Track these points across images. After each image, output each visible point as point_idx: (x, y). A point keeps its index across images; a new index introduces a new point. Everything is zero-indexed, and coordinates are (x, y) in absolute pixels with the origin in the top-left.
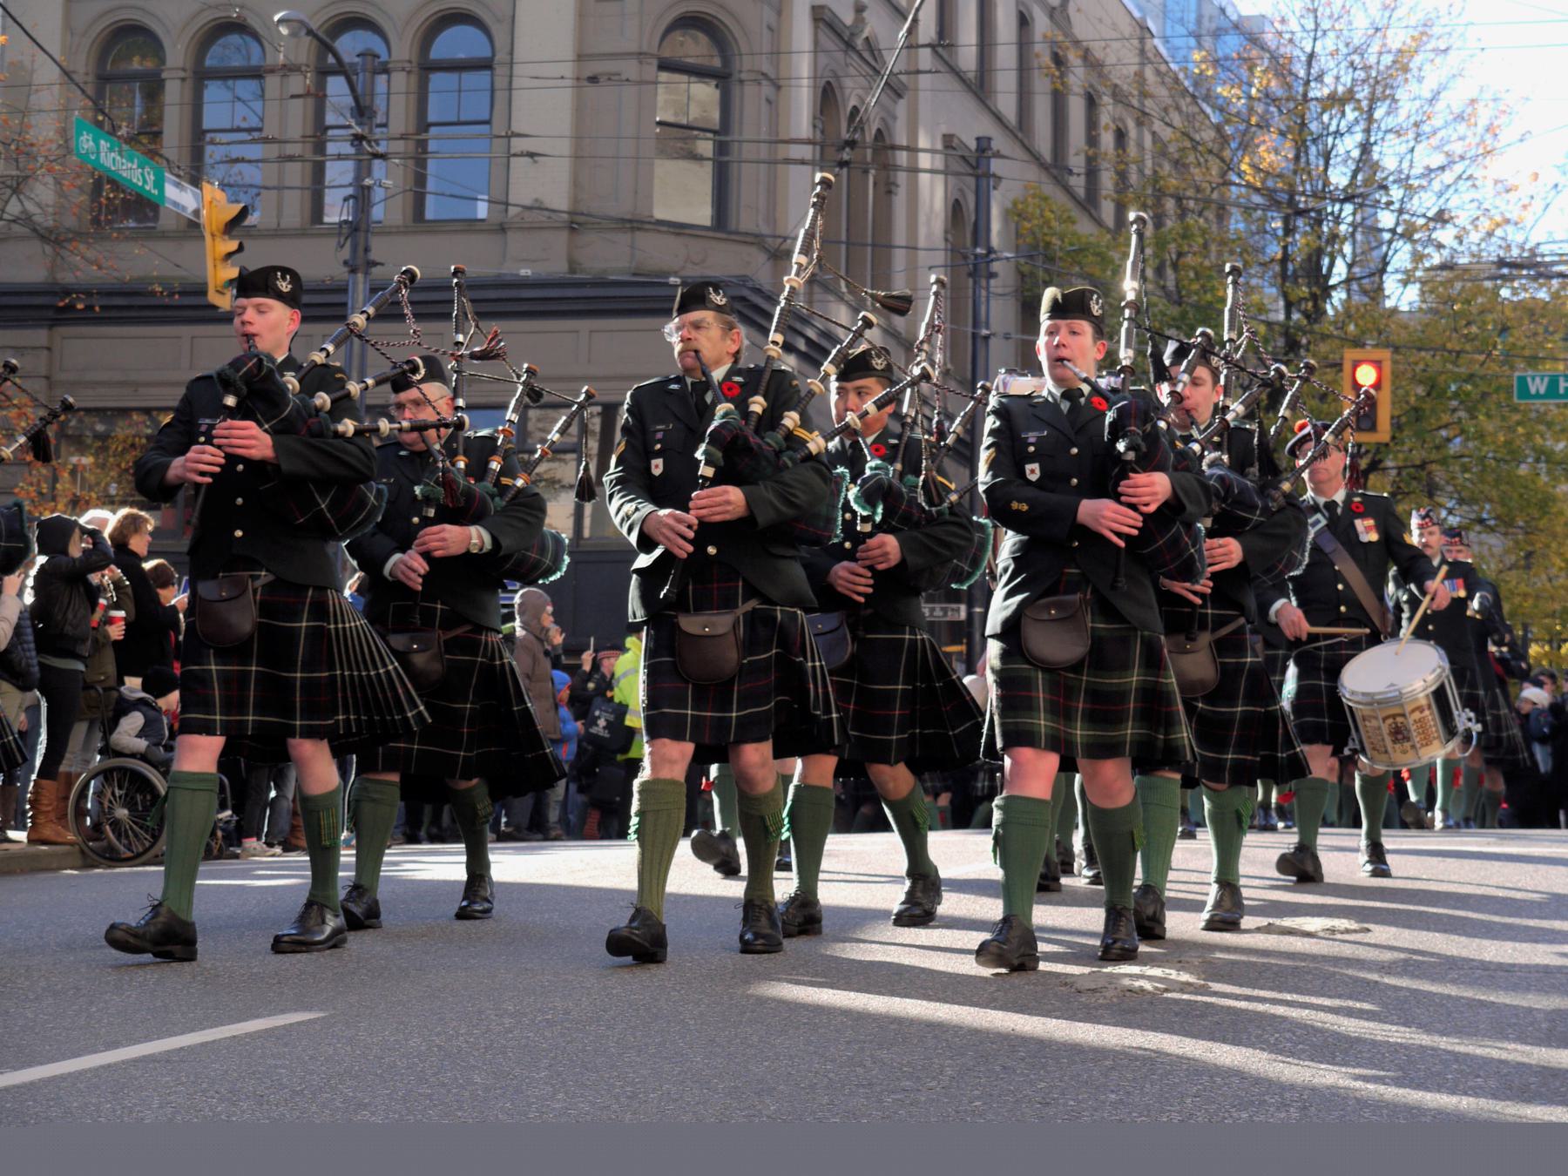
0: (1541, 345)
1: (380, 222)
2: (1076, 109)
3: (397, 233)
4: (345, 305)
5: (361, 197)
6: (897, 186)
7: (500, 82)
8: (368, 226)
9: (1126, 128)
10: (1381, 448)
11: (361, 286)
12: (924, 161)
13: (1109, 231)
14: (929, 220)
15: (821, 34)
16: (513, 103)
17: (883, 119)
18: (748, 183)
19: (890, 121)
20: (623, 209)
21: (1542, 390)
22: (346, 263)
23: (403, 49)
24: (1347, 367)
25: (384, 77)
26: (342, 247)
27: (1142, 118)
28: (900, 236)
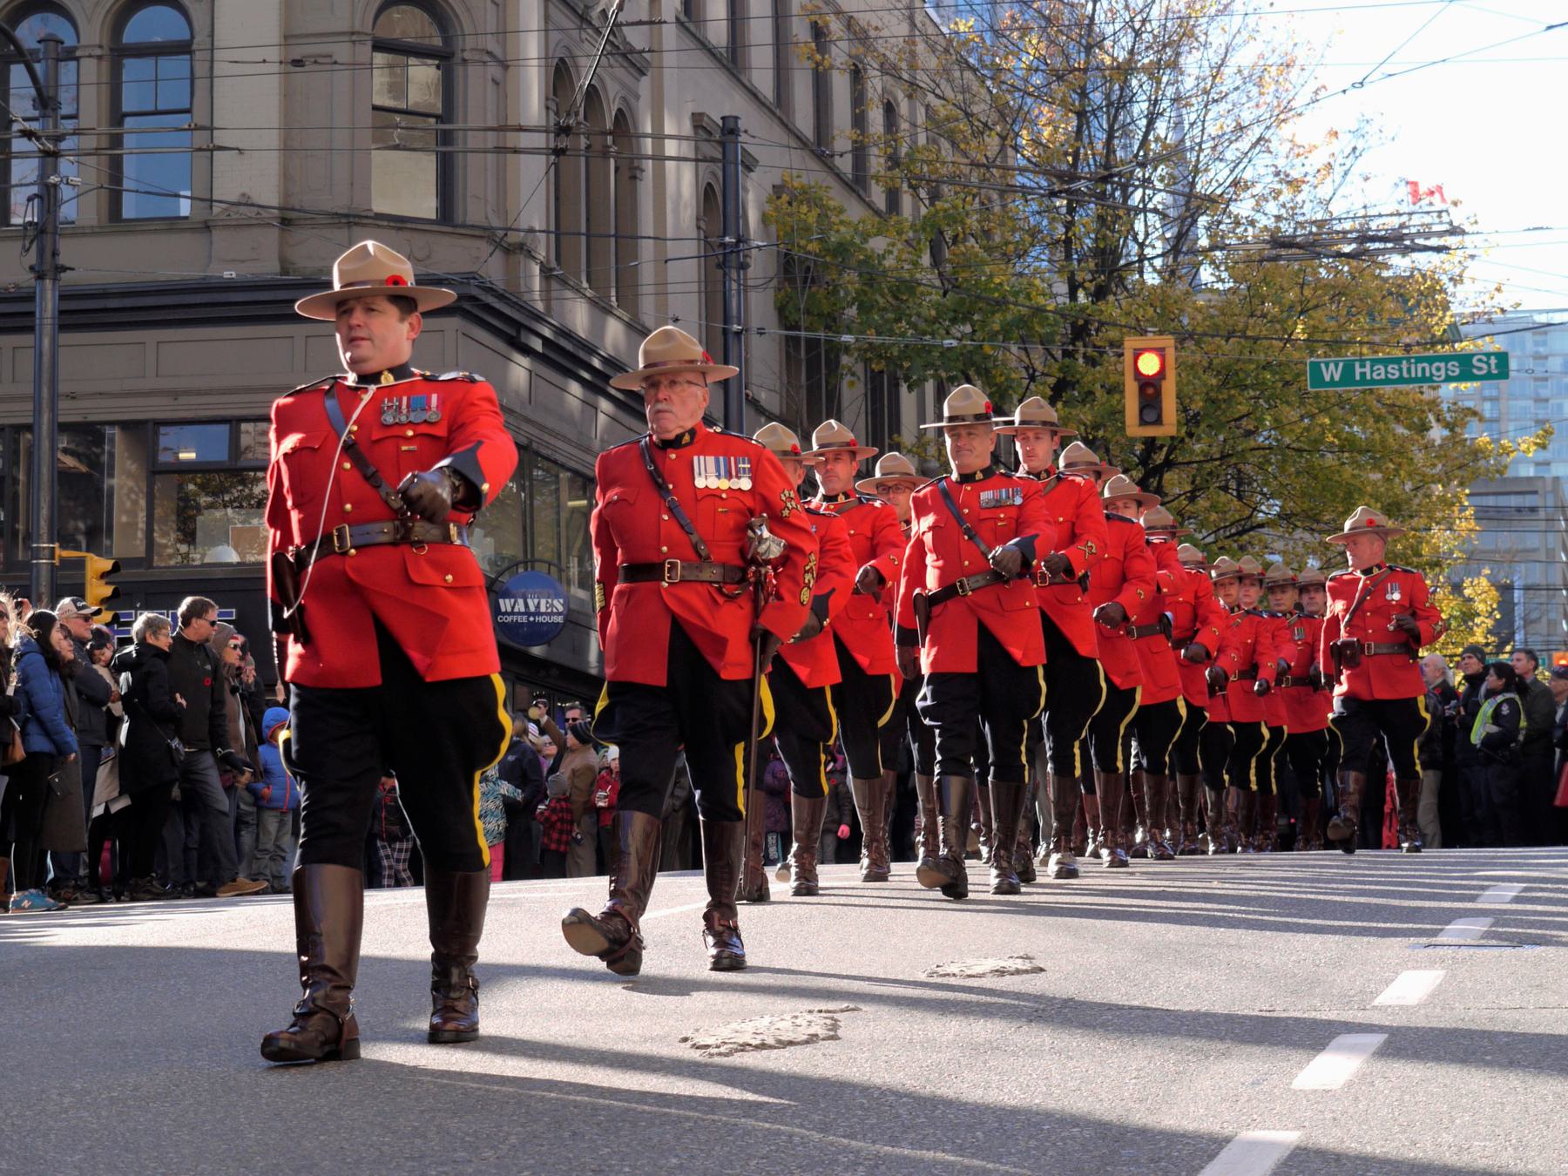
0: (1342, 327)
1: (73, 223)
2: (840, 86)
3: (94, 234)
4: (32, 314)
5: (48, 196)
6: (643, 171)
7: (201, 69)
8: (56, 227)
9: (896, 100)
10: (1175, 443)
11: (49, 295)
12: (671, 148)
13: (877, 212)
14: (676, 211)
15: (552, 9)
16: (215, 89)
17: (624, 99)
18: (475, 175)
19: (632, 101)
20: (338, 203)
21: (1337, 378)
22: (32, 268)
23: (93, 32)
24: (1128, 356)
25: (73, 64)
26: (28, 250)
27: (913, 88)
28: (647, 226)
